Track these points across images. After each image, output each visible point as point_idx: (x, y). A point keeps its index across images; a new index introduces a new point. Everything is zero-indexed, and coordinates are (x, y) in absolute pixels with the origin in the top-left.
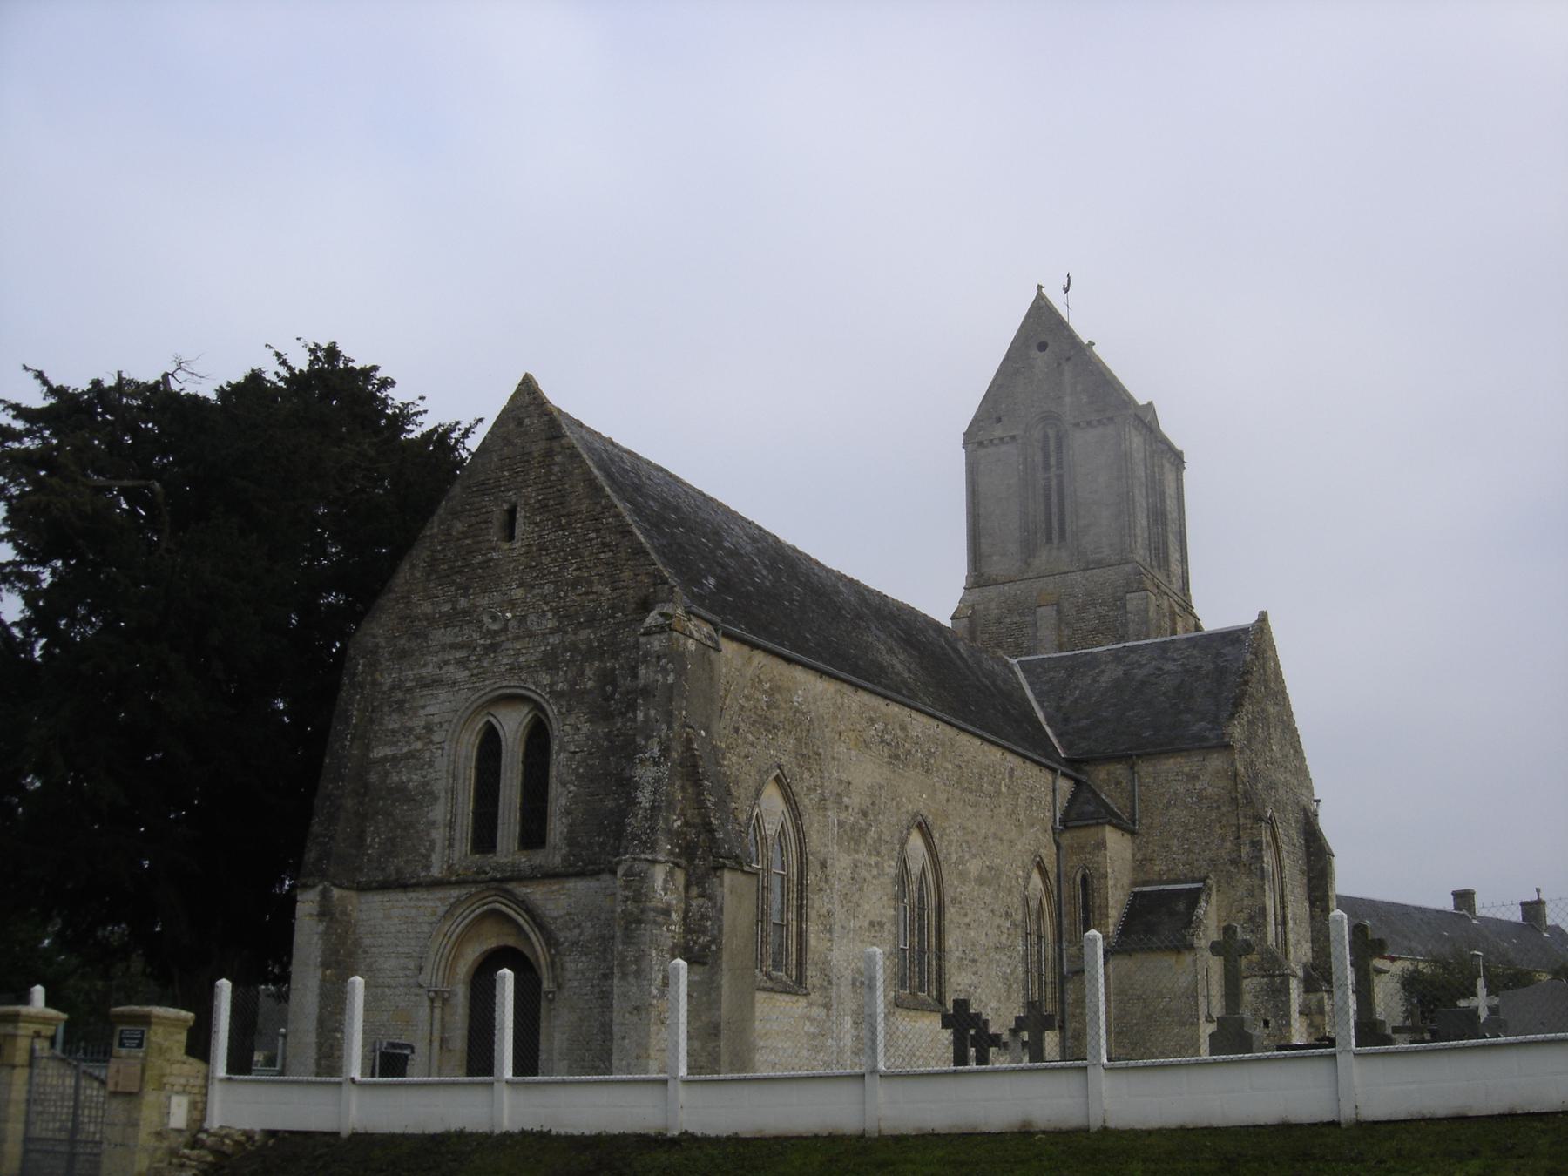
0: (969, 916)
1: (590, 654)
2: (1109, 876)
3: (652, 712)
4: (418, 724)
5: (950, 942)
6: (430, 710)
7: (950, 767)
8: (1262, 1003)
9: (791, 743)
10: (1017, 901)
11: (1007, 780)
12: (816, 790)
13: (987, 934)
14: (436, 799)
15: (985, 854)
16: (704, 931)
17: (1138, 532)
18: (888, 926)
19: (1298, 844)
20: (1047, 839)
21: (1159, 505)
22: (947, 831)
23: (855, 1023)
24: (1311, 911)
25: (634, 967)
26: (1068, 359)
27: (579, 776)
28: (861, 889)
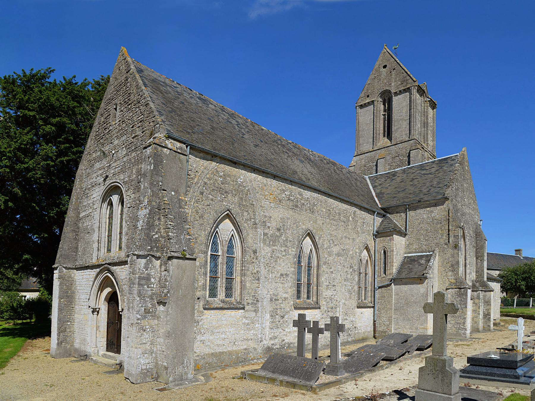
0: (332, 268)
2: (394, 251)
5: (322, 279)
6: (94, 196)
7: (324, 210)
8: (455, 299)
9: (236, 200)
10: (355, 261)
11: (352, 215)
12: (251, 220)
13: (341, 275)
15: (341, 244)
17: (417, 128)
18: (291, 275)
19: (473, 236)
21: (425, 121)
22: (323, 236)
23: (271, 316)
24: (476, 261)
28: (276, 261)
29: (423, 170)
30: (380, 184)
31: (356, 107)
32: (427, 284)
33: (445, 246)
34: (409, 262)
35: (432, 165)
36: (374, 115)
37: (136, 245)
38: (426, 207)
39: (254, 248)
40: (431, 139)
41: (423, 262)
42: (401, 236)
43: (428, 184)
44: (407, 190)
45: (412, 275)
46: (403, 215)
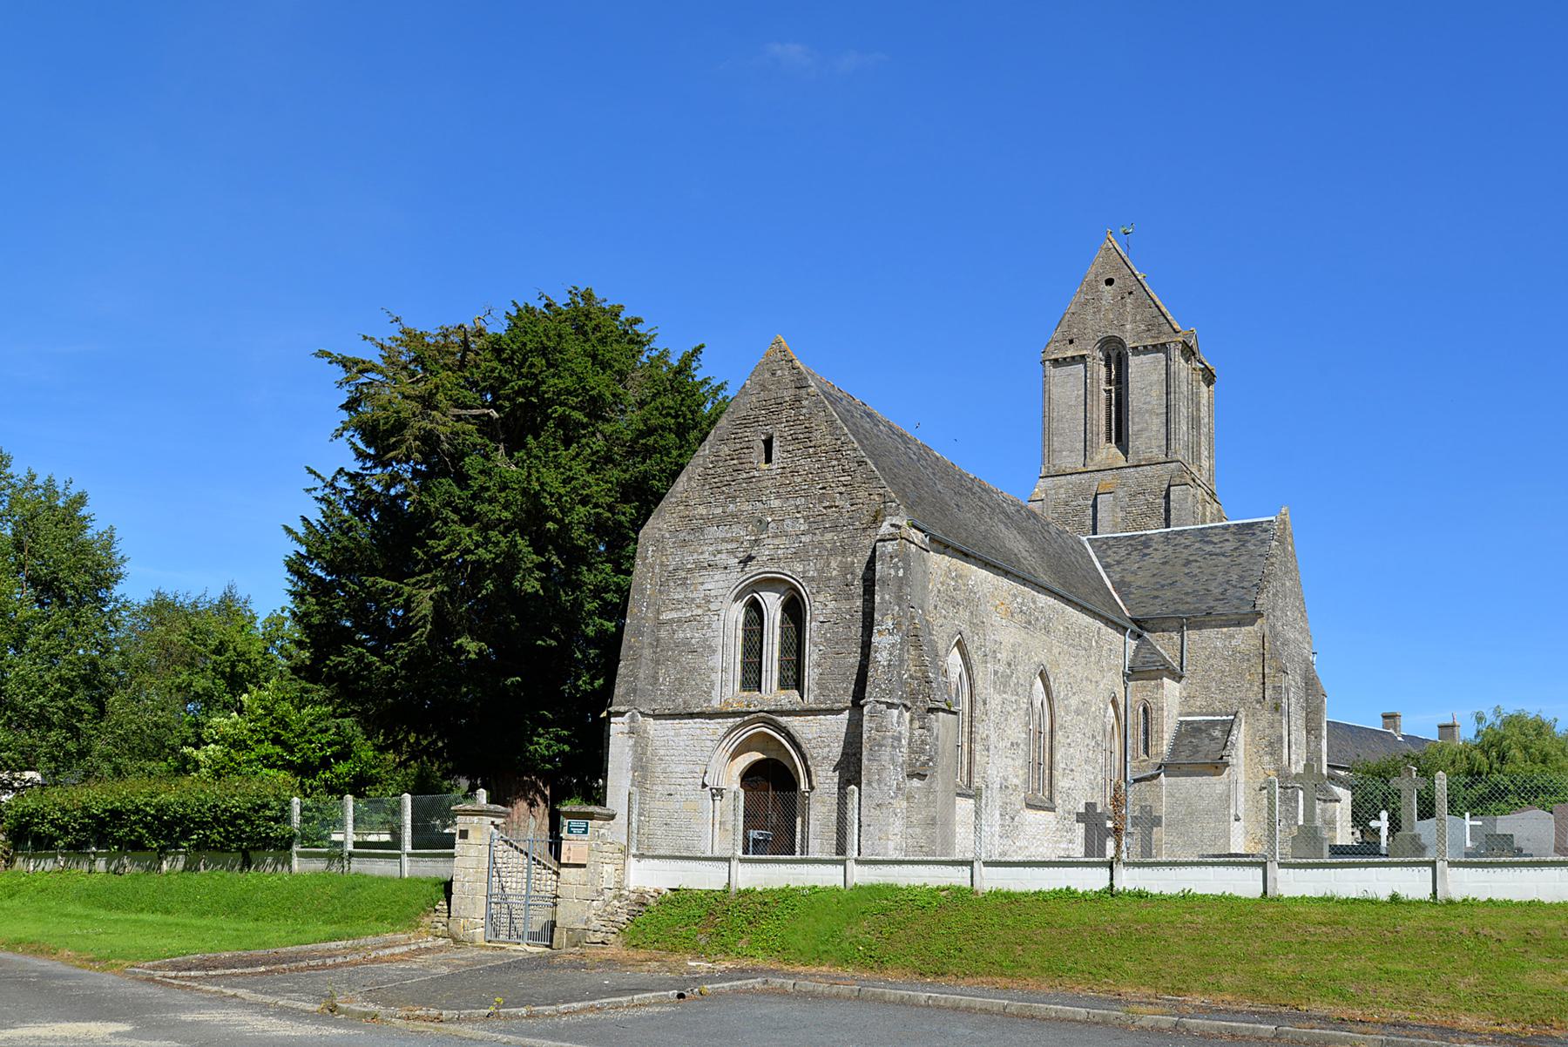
1: (833, 552)
3: (887, 597)
4: (698, 595)
5: (1058, 757)
6: (707, 586)
7: (1062, 629)
14: (714, 651)
16: (923, 752)
18: (1022, 746)
20: (1119, 680)
23: (1001, 815)
25: (877, 777)
26: (1130, 293)
27: (827, 640)
28: (1006, 720)
29: (1207, 542)
30: (1119, 563)
31: (1044, 361)
32: (1229, 775)
33: (1258, 706)
34: (1189, 732)
35: (1223, 534)
36: (1086, 390)
37: (881, 688)
38: (1220, 627)
39: (983, 696)
40: (1206, 453)
41: (1217, 733)
42: (1174, 679)
43: (1220, 578)
44: (1178, 584)
45: (1200, 758)
46: (1176, 636)
